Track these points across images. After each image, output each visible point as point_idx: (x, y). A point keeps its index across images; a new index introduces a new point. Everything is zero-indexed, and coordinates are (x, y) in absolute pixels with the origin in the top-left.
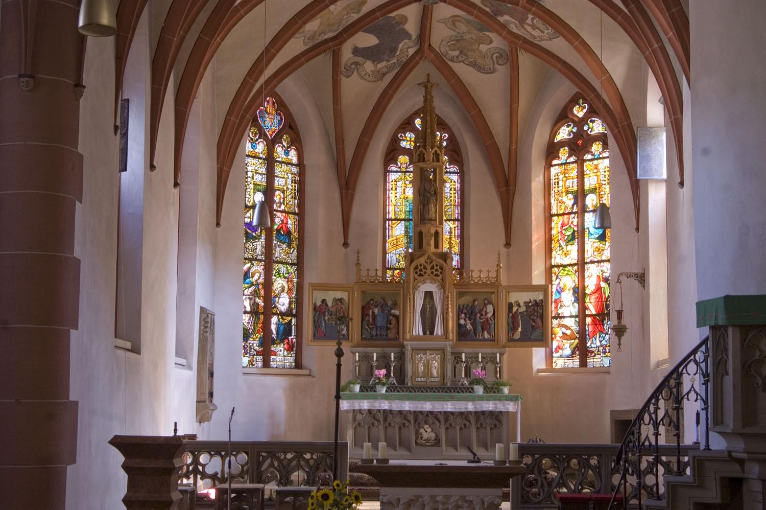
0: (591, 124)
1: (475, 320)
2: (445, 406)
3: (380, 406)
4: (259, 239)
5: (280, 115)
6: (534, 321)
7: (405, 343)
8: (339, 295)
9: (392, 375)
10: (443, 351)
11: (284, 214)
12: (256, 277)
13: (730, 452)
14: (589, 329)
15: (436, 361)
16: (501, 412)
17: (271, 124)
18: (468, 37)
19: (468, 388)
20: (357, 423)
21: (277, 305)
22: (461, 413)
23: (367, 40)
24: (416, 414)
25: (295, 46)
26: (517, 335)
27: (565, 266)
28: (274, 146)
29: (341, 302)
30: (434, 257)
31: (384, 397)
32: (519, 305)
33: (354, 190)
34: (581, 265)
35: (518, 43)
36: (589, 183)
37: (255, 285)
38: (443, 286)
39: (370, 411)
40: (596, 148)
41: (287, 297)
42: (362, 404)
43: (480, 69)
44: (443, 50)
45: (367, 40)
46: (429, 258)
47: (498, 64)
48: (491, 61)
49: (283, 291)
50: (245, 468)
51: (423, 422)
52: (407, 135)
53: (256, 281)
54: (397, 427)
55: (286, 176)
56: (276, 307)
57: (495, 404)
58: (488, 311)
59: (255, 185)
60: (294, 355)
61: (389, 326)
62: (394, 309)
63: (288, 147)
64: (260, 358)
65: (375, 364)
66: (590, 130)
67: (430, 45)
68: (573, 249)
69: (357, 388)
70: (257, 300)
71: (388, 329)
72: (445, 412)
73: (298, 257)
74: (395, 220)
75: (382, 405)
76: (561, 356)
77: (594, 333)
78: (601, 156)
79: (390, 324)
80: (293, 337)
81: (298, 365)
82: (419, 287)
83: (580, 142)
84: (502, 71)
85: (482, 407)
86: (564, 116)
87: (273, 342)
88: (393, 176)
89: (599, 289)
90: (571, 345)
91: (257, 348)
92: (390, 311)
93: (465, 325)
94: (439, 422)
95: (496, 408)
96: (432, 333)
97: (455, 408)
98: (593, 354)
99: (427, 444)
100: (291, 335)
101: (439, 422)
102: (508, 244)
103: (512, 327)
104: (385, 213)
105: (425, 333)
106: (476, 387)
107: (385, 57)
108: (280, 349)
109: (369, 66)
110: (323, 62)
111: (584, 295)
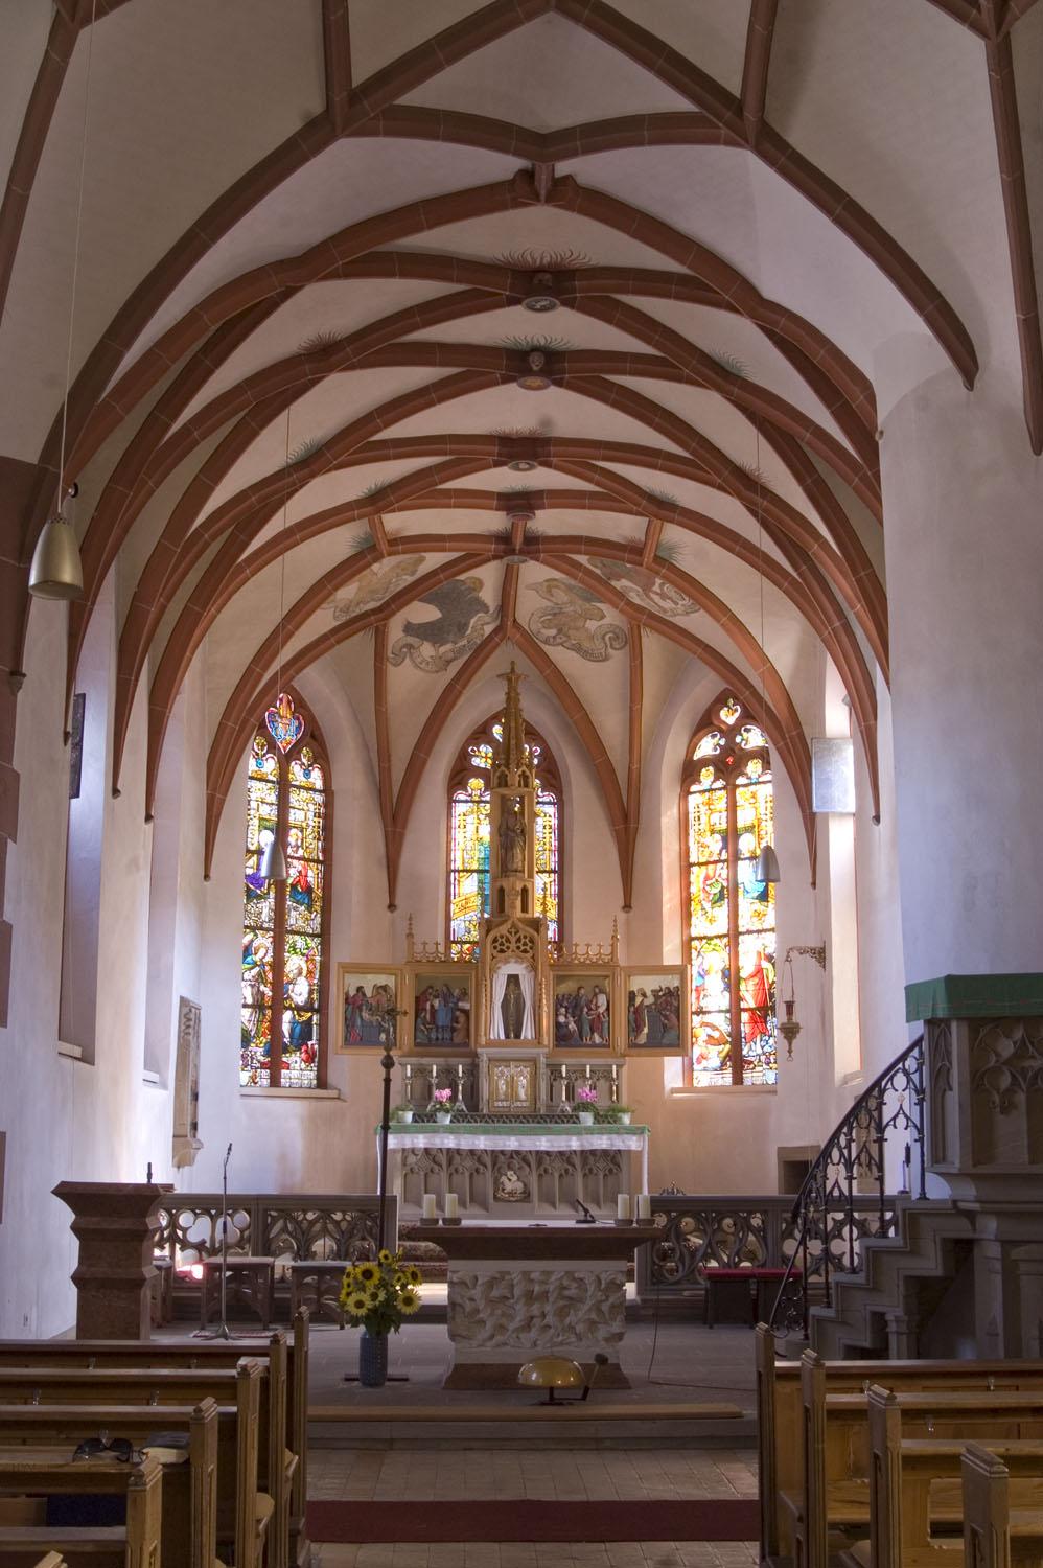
0: (745, 735)
1: (580, 1016)
2: (538, 1143)
3: (443, 1143)
4: (265, 899)
5: (298, 719)
6: (666, 1017)
7: (479, 1050)
8: (382, 980)
9: (460, 1097)
10: (534, 1061)
11: (302, 862)
12: (261, 953)
15: (524, 1077)
16: (619, 1150)
17: (285, 731)
19: (571, 1116)
20: (408, 1168)
21: (292, 995)
24: (495, 1155)
25: (322, 621)
26: (642, 1039)
27: (710, 938)
28: (289, 763)
29: (385, 991)
30: (521, 925)
31: (449, 1130)
32: (644, 995)
33: (404, 827)
34: (734, 936)
35: (641, 619)
36: (744, 818)
37: (259, 966)
38: (534, 968)
39: (427, 1150)
40: (754, 768)
41: (307, 983)
42: (415, 1141)
43: (587, 655)
44: (534, 628)
45: (423, 612)
46: (514, 925)
47: (612, 647)
48: (603, 645)
49: (300, 974)
50: (246, 1233)
51: (505, 1166)
52: (480, 749)
53: (261, 960)
54: (467, 1174)
55: (306, 808)
56: (289, 998)
57: (610, 1139)
58: (599, 1004)
59: (261, 819)
60: (315, 1069)
61: (455, 1025)
62: (462, 1001)
63: (310, 766)
64: (266, 1073)
65: (434, 1081)
66: (744, 742)
67: (515, 620)
68: (722, 913)
69: (409, 1116)
70: (262, 988)
71: (453, 1030)
72: (538, 1152)
73: (322, 925)
74: (463, 871)
75: (446, 1141)
76: (705, 1069)
77: (753, 1035)
78: (760, 780)
80: (313, 1042)
81: (322, 1082)
82: (499, 968)
84: (618, 658)
85: (592, 1144)
86: (706, 723)
87: (286, 1050)
88: (460, 809)
89: (759, 971)
91: (262, 1059)
92: (456, 1004)
93: (567, 1024)
94: (529, 1165)
95: (612, 1145)
96: (518, 1036)
97: (553, 1146)
98: (752, 1066)
99: (512, 1199)
100: (311, 1040)
101: (529, 1165)
102: (627, 907)
103: (635, 1027)
104: (448, 862)
105: (507, 1036)
107: (451, 637)
109: (427, 650)
110: (360, 645)
111: (738, 980)
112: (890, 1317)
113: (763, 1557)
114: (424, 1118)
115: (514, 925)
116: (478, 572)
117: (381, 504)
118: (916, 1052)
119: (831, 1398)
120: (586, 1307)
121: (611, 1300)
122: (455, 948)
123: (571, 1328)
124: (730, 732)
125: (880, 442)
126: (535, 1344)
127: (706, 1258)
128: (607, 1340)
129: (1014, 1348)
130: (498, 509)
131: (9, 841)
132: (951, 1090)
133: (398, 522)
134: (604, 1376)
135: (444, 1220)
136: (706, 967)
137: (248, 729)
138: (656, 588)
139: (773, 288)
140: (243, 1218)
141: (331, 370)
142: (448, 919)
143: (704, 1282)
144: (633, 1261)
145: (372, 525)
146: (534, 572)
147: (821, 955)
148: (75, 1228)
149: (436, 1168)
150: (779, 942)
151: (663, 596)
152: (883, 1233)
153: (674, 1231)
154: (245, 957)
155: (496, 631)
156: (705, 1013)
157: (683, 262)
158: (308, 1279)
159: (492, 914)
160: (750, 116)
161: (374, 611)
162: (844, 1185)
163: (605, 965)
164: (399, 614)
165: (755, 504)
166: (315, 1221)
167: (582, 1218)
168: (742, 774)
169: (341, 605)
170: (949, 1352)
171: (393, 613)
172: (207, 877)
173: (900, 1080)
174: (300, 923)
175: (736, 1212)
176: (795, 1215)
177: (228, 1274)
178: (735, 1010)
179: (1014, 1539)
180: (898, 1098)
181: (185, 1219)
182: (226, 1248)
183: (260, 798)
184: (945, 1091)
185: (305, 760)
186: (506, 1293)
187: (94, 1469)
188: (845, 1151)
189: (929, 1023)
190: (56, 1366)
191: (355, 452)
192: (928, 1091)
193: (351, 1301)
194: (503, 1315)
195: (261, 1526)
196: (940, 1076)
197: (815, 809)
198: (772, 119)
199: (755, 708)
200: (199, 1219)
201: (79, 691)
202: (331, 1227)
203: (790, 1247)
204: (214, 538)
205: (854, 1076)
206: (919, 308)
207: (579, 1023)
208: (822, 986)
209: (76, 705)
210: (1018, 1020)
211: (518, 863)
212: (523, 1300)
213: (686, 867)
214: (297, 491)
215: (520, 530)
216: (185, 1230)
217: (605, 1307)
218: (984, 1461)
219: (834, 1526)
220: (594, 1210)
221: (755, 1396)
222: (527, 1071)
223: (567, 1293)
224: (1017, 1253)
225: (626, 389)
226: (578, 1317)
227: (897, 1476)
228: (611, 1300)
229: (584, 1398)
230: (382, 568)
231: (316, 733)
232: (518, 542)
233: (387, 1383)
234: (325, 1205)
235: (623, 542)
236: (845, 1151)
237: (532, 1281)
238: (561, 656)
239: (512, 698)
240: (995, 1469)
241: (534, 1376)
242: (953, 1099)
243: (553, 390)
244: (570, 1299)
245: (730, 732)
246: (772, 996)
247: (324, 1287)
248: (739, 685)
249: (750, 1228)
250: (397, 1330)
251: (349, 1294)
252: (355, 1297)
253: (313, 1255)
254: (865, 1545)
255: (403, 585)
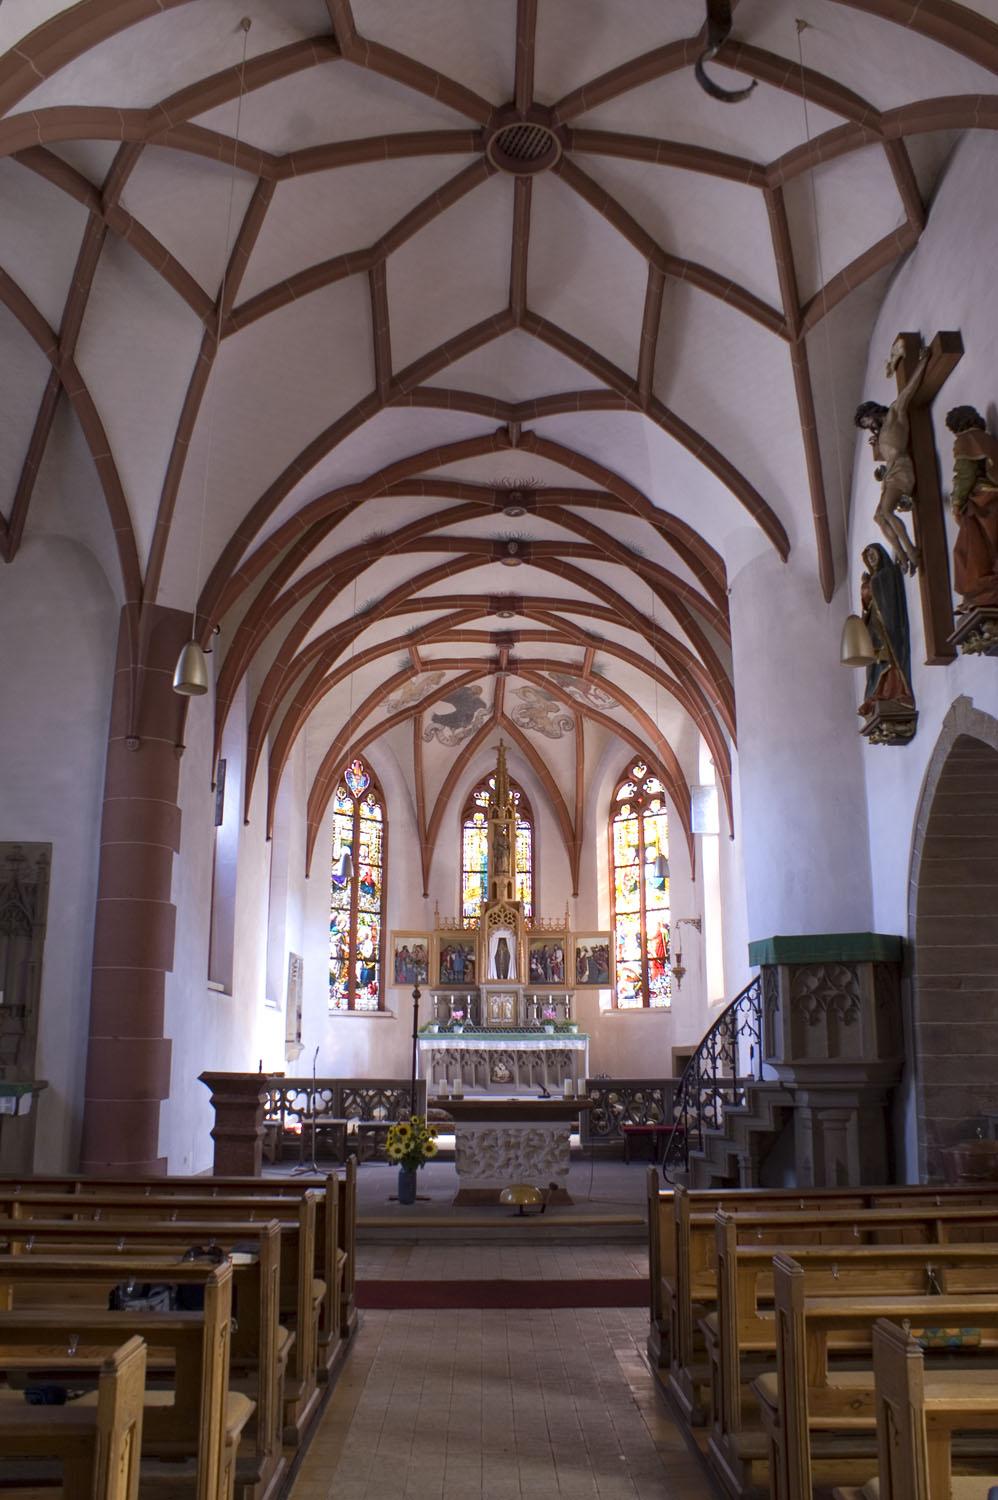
6: (600, 965)
7: (481, 986)
10: (516, 994)
13: (781, 1083)
14: (651, 972)
17: (357, 784)
18: (537, 705)
20: (435, 1062)
22: (534, 1052)
23: (444, 708)
25: (379, 714)
26: (585, 978)
27: (628, 914)
30: (507, 907)
31: (461, 1037)
32: (586, 951)
33: (433, 844)
34: (643, 912)
35: (583, 711)
38: (515, 934)
39: (448, 1050)
40: (655, 805)
43: (549, 734)
44: (514, 717)
45: (444, 708)
46: (503, 907)
49: (367, 938)
50: (330, 1104)
51: (497, 1061)
54: (473, 1066)
56: (360, 953)
64: (345, 1001)
65: (452, 1006)
67: (503, 713)
69: (436, 1029)
71: (465, 973)
73: (381, 907)
77: (656, 975)
79: (467, 969)
81: (381, 1007)
83: (640, 800)
84: (569, 737)
86: (625, 777)
87: (358, 986)
88: (467, 832)
90: (635, 987)
94: (513, 1060)
96: (505, 977)
101: (513, 1060)
102: (575, 894)
103: (580, 971)
104: (462, 866)
105: (499, 977)
106: (546, 1027)
107: (462, 724)
108: (364, 992)
109: (447, 732)
110: (406, 728)
111: (646, 940)
112: (740, 1158)
113: (652, 1319)
114: (446, 1030)
115: (503, 907)
116: (478, 683)
117: (416, 640)
118: (755, 986)
119: (693, 1216)
120: (544, 1153)
121: (561, 1148)
122: (466, 921)
123: (535, 1166)
124: (640, 783)
125: (730, 596)
126: (511, 1176)
127: (626, 1118)
128: (559, 1173)
129: (821, 1180)
130: (491, 642)
131: (175, 853)
132: (778, 1010)
133: (427, 651)
134: (555, 1197)
135: (453, 1096)
136: (626, 932)
137: (334, 781)
138: (592, 691)
139: (661, 500)
140: (327, 1095)
141: (382, 554)
142: (462, 902)
143: (624, 1135)
144: (577, 1120)
145: (411, 653)
146: (514, 682)
147: (698, 924)
148: (213, 1102)
149: (454, 1062)
150: (672, 915)
151: (596, 697)
152: (737, 1103)
153: (603, 1102)
154: (332, 927)
155: (491, 720)
156: (625, 961)
157: (603, 484)
158: (370, 1133)
159: (489, 900)
160: (643, 391)
161: (416, 706)
162: (711, 1072)
163: (561, 932)
164: (429, 709)
165: (652, 637)
166: (374, 1096)
167: (542, 1094)
168: (648, 809)
169: (392, 703)
170: (779, 1183)
171: (425, 709)
172: (307, 876)
173: (746, 1004)
174: (367, 905)
175: (644, 1090)
176: (680, 1091)
177: (318, 1130)
178: (645, 961)
179: (808, 1318)
180: (746, 1016)
181: (291, 1095)
182: (317, 1113)
183: (342, 826)
184: (774, 1012)
185: (370, 802)
186: (493, 1143)
187: (197, 1268)
188: (711, 1051)
189: (765, 967)
190: (194, 1194)
191: (400, 606)
192: (763, 1011)
193: (392, 1149)
194: (491, 1157)
195: (317, 1302)
196: (771, 1001)
197: (693, 831)
198: (658, 394)
199: (658, 770)
200: (300, 1095)
201: (223, 758)
202: (384, 1099)
203: (678, 1111)
204: (309, 660)
205: (719, 1001)
206: (752, 511)
207: (545, 968)
208: (700, 944)
209: (220, 767)
210: (822, 964)
211: (505, 867)
212: (503, 1148)
213: (613, 869)
214: (362, 631)
215: (505, 658)
216: (291, 1102)
217: (557, 1152)
218: (787, 1265)
219: (696, 1301)
220: (551, 1088)
221: (646, 1209)
222: (511, 1000)
223: (532, 1143)
224: (821, 1116)
225: (572, 566)
226: (539, 1158)
227: (734, 1270)
228: (561, 1148)
229: (542, 1211)
230: (418, 680)
231: (378, 785)
232: (504, 662)
233: (417, 1202)
234: (380, 1086)
235: (569, 662)
236: (711, 1051)
237: (509, 1135)
238: (529, 733)
239: (501, 762)
240: (794, 1270)
241: (510, 1197)
242: (780, 1016)
243: (523, 566)
244: (534, 1147)
245: (640, 783)
246: (668, 950)
247: (379, 1138)
248: (646, 753)
249: (653, 1099)
250: (422, 1167)
251: (391, 1145)
252: (395, 1146)
253: (373, 1118)
254: (714, 1316)
255: (432, 691)
